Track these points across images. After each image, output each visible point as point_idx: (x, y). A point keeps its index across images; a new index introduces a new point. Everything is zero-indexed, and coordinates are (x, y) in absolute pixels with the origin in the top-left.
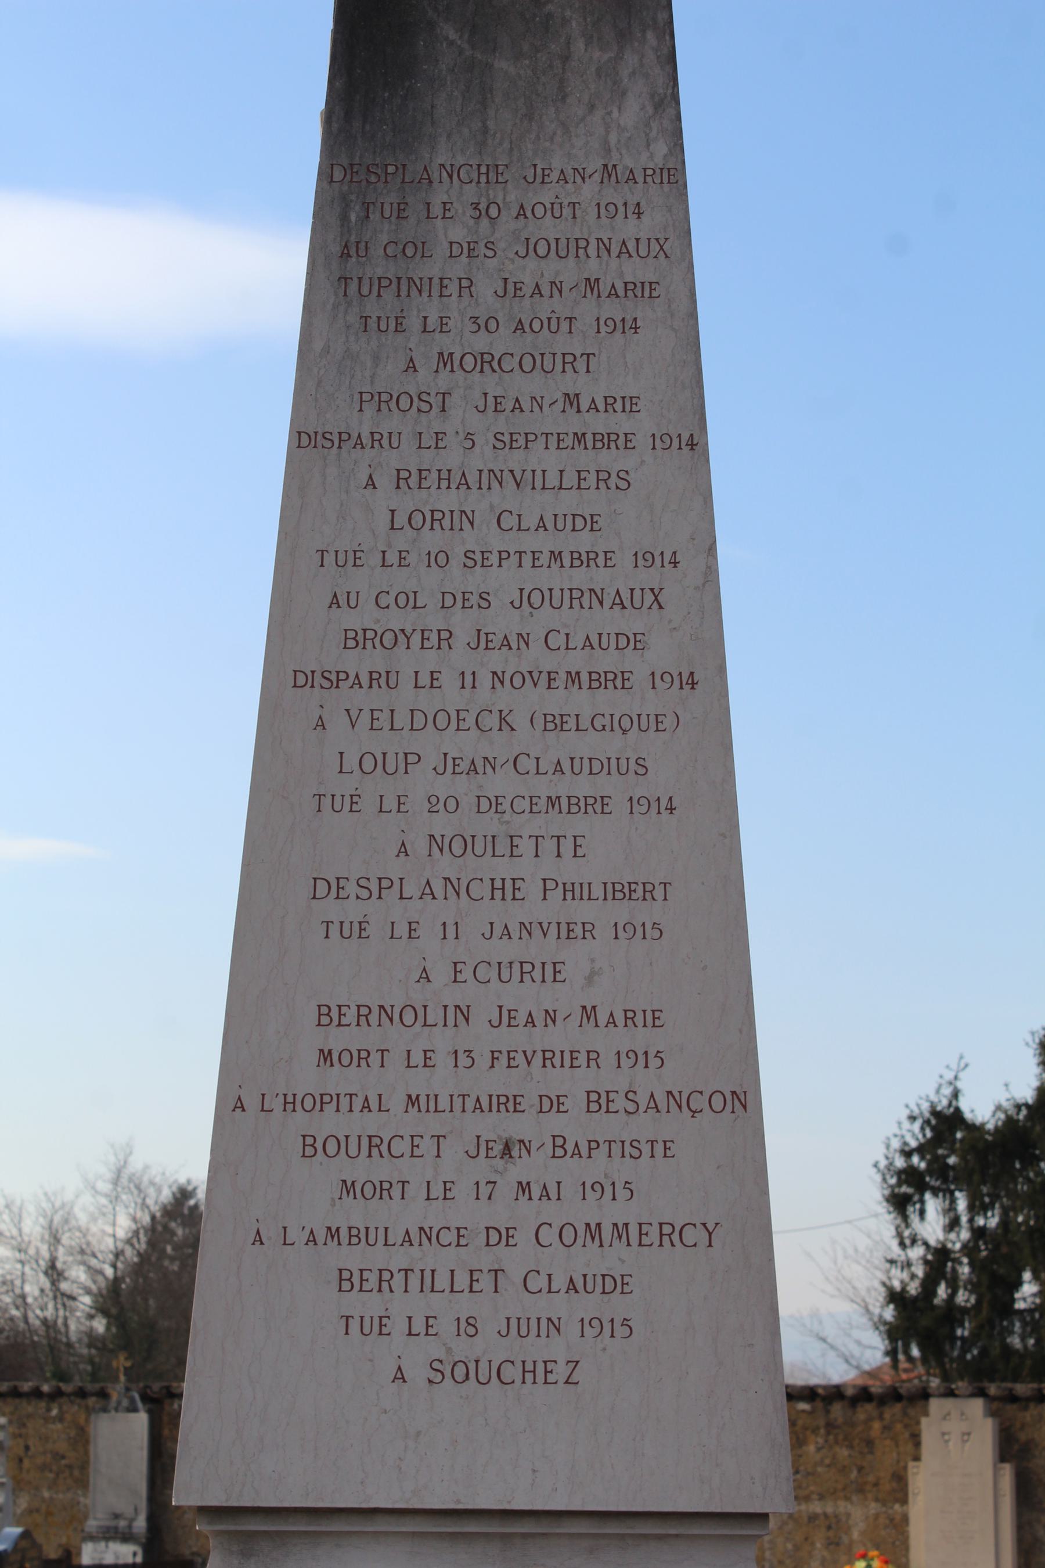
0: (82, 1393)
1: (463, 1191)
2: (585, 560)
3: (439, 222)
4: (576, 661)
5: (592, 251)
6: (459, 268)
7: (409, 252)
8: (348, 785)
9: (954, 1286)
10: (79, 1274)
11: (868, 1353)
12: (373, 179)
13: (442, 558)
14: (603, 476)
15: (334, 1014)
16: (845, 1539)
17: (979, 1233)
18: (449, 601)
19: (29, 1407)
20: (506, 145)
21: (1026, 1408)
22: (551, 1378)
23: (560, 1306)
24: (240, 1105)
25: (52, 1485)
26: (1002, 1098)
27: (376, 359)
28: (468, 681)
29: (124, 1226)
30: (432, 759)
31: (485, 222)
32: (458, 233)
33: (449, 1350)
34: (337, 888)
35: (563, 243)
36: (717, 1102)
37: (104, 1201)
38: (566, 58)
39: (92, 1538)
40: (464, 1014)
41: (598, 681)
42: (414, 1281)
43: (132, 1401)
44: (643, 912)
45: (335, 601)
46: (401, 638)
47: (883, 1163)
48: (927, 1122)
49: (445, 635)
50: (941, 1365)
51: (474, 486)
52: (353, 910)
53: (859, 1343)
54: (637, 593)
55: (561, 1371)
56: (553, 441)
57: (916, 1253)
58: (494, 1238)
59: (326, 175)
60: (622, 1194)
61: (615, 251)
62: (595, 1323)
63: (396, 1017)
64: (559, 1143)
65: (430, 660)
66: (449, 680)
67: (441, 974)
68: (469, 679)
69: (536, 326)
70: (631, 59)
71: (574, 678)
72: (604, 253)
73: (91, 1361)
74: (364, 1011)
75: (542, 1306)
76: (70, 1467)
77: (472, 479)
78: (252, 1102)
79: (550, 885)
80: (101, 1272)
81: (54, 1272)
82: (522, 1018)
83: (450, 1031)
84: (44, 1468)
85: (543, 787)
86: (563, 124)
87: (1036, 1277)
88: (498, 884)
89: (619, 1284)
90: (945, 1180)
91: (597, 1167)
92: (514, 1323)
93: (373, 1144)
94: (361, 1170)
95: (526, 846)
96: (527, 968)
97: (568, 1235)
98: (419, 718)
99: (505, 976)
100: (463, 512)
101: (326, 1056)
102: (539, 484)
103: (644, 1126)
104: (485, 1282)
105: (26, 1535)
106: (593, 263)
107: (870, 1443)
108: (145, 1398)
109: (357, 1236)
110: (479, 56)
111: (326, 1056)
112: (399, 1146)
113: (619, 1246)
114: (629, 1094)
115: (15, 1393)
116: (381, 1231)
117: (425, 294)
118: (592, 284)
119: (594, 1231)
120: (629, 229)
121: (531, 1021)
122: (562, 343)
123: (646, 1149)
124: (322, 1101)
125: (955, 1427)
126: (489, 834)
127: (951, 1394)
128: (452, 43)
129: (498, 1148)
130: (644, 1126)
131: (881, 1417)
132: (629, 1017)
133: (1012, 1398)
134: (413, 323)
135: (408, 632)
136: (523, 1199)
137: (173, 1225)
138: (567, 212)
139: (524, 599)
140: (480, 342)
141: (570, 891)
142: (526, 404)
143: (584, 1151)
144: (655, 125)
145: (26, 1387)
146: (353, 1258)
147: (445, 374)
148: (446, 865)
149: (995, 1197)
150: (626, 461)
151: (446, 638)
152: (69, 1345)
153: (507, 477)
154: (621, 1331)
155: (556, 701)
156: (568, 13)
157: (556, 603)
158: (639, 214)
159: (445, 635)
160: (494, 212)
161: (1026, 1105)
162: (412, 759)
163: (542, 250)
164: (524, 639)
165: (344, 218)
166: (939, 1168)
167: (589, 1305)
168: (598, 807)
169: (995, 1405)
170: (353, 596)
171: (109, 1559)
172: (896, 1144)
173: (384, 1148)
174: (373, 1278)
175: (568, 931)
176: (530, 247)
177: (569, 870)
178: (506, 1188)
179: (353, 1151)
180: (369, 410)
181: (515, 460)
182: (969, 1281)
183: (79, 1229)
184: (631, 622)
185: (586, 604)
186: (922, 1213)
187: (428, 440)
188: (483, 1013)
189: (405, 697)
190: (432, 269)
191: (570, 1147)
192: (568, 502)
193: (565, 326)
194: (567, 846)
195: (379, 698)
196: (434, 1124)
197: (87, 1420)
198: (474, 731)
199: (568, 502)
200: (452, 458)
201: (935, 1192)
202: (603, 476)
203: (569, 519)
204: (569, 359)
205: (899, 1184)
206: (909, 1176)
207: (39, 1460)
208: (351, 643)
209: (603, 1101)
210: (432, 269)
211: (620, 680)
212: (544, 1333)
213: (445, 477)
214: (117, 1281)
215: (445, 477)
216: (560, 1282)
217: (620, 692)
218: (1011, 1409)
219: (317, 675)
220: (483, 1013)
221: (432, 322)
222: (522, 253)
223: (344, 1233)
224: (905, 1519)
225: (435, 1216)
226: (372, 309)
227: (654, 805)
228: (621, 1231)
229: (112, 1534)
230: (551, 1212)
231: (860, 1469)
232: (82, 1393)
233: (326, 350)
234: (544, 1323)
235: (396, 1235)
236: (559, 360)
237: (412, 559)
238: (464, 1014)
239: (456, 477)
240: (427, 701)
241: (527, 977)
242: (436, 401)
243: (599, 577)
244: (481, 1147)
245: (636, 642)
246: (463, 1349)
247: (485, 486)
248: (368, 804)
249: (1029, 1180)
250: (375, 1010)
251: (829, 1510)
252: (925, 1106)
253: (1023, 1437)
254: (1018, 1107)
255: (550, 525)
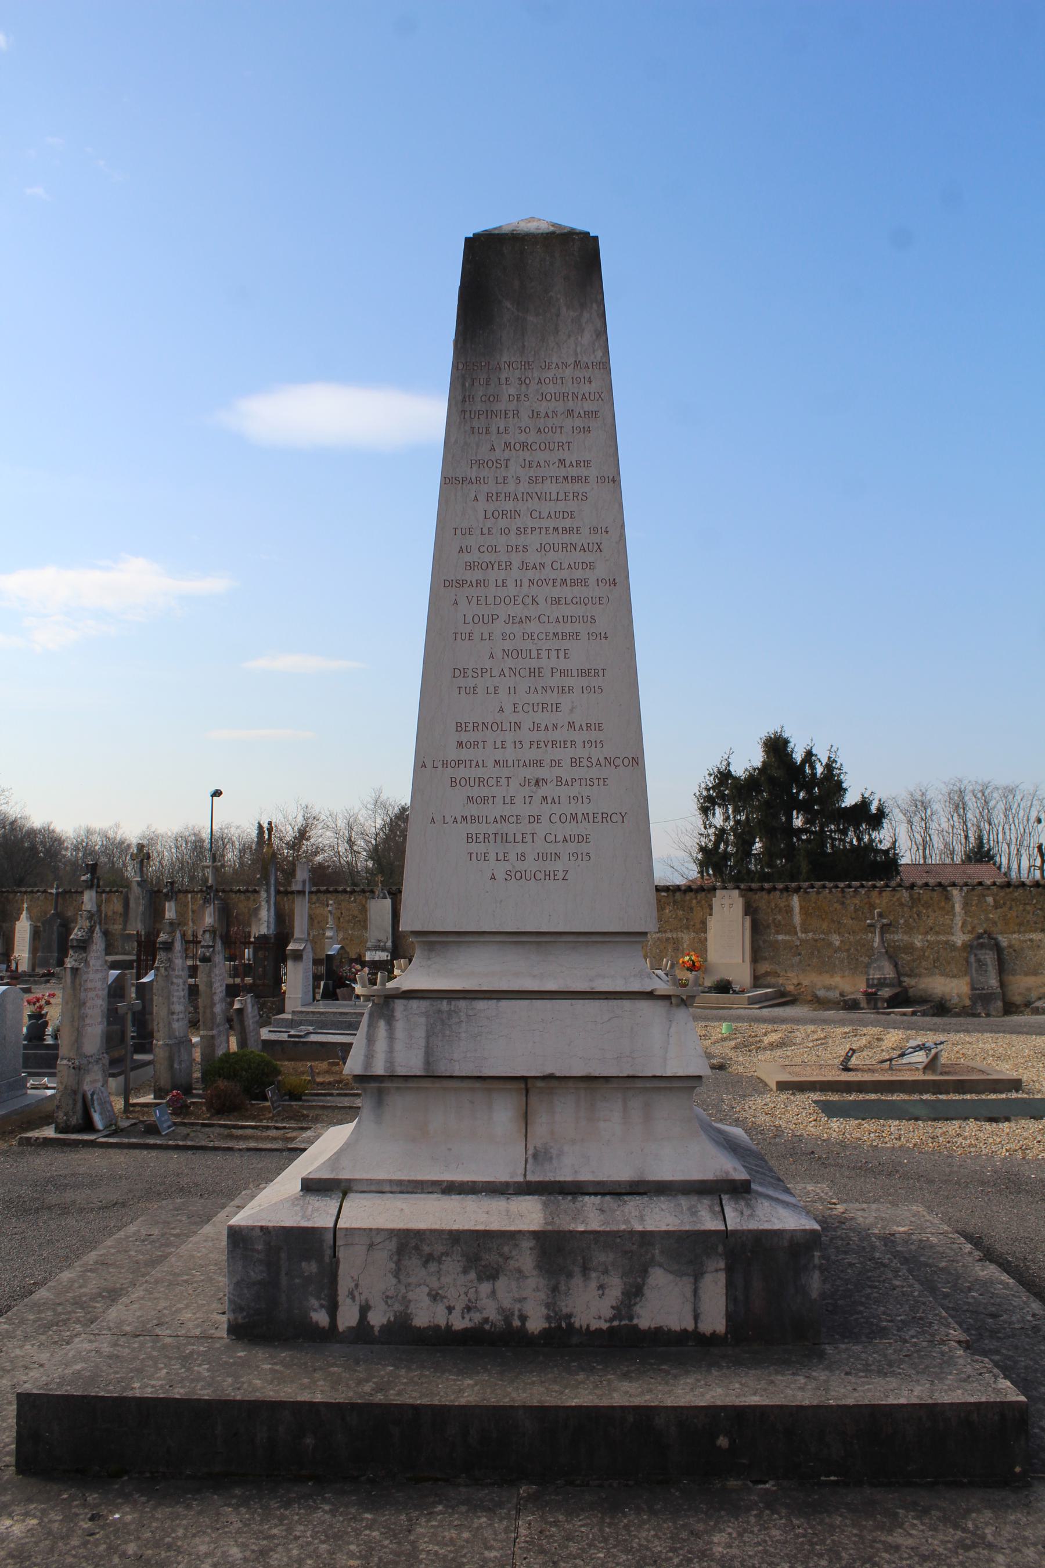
0: (363, 891)
1: (519, 800)
2: (569, 531)
3: (504, 386)
4: (565, 574)
5: (570, 398)
6: (512, 406)
7: (492, 399)
8: (468, 628)
9: (727, 844)
10: (361, 843)
11: (691, 872)
12: (476, 368)
13: (507, 531)
14: (576, 494)
15: (463, 726)
16: (681, 948)
17: (737, 822)
18: (510, 549)
19: (342, 897)
20: (533, 353)
21: (756, 894)
22: (556, 878)
23: (559, 848)
24: (424, 765)
25: (353, 929)
26: (748, 766)
27: (478, 446)
28: (518, 583)
29: (379, 823)
30: (503, 617)
31: (524, 386)
32: (512, 391)
33: (514, 867)
34: (464, 672)
35: (557, 395)
36: (626, 762)
37: (371, 812)
38: (558, 315)
39: (369, 950)
40: (518, 725)
41: (574, 583)
42: (499, 838)
43: (384, 894)
44: (595, 682)
45: (461, 550)
46: (490, 565)
47: (698, 794)
48: (717, 776)
49: (508, 564)
50: (722, 877)
51: (520, 500)
52: (470, 682)
53: (687, 868)
54: (591, 545)
55: (561, 875)
56: (554, 480)
57: (712, 831)
58: (532, 820)
59: (455, 366)
60: (586, 801)
61: (580, 398)
62: (575, 855)
63: (489, 727)
64: (559, 779)
65: (503, 574)
66: (510, 583)
67: (508, 709)
68: (519, 583)
69: (546, 430)
70: (586, 315)
71: (564, 582)
72: (575, 399)
73: (367, 878)
74: (476, 725)
75: (552, 848)
76: (359, 921)
77: (519, 496)
78: (429, 764)
79: (555, 670)
80: (370, 842)
81: (351, 842)
82: (543, 727)
83: (512, 733)
84: (349, 922)
85: (551, 629)
86: (557, 344)
87: (761, 840)
88: (532, 670)
89: (585, 839)
90: (724, 801)
91: (575, 790)
92: (541, 855)
93: (480, 781)
94: (476, 792)
95: (544, 654)
96: (545, 706)
97: (563, 819)
98: (498, 600)
99: (536, 709)
100: (515, 511)
101: (460, 744)
102: (548, 498)
103: (594, 773)
104: (529, 838)
105: (342, 948)
106: (571, 402)
107: (691, 909)
108: (390, 893)
109: (473, 819)
110: (520, 314)
111: (460, 744)
112: (492, 782)
113: (585, 823)
114: (589, 759)
115: (336, 891)
116: (484, 818)
117: (498, 417)
118: (570, 412)
119: (574, 817)
120: (586, 388)
121: (547, 728)
122: (558, 438)
123: (596, 782)
124: (459, 763)
125: (727, 902)
126: (528, 649)
127: (725, 888)
128: (508, 309)
129: (533, 782)
130: (594, 773)
131: (696, 898)
132: (589, 726)
133: (750, 890)
134: (493, 429)
135: (493, 562)
136: (544, 803)
137: (400, 823)
138: (559, 381)
139: (542, 548)
140: (522, 438)
141: (563, 673)
142: (542, 464)
143: (570, 783)
144: (597, 344)
145: (340, 888)
146: (473, 829)
147: (507, 452)
148: (510, 662)
149: (744, 808)
150: (586, 488)
151: (509, 565)
152: (358, 872)
153: (534, 496)
154: (586, 858)
155: (557, 592)
156: (559, 296)
157: (556, 549)
158: (590, 382)
159: (508, 564)
160: (528, 381)
161: (758, 768)
162: (495, 617)
163: (548, 398)
164: (543, 565)
165: (463, 385)
166: (722, 796)
167: (572, 847)
168: (575, 637)
169: (743, 892)
170: (469, 548)
171: (377, 958)
172: (703, 785)
173: (485, 783)
174: (481, 837)
175: (562, 690)
176: (543, 397)
177: (563, 664)
178: (537, 799)
179: (472, 784)
180: (475, 467)
181: (538, 488)
182: (733, 842)
183: (361, 824)
184: (589, 557)
185: (569, 550)
186: (714, 814)
187: (501, 480)
188: (527, 725)
189: (492, 590)
190: (501, 406)
191: (564, 781)
192: (561, 506)
193: (559, 430)
194: (562, 654)
195: (480, 591)
196: (506, 772)
197: (366, 902)
198: (521, 605)
199: (561, 506)
200: (511, 487)
201: (720, 805)
202: (576, 494)
203: (561, 513)
204: (561, 444)
205: (704, 802)
206: (709, 799)
207: (347, 918)
208: (468, 568)
209: (578, 762)
210: (501, 406)
211: (584, 582)
212: (553, 859)
213: (508, 496)
214: (377, 845)
215: (508, 496)
216: (560, 838)
217: (584, 587)
218: (750, 894)
219: (454, 582)
220: (527, 725)
221: (502, 429)
222: (540, 399)
223: (469, 818)
224: (706, 939)
225: (507, 811)
226: (476, 424)
227: (599, 636)
228: (585, 816)
229: (377, 948)
230: (555, 808)
231: (687, 919)
232: (363, 891)
233: (456, 442)
234: (553, 855)
235: (491, 819)
236: (556, 444)
237: (494, 531)
238: (518, 725)
239: (512, 496)
240: (501, 592)
241: (545, 710)
242: (503, 463)
243: (574, 538)
244: (526, 782)
245: (591, 566)
246: (520, 866)
247: (525, 499)
248: (476, 636)
249: (759, 800)
250: (481, 724)
251: (674, 936)
252: (716, 769)
253: (754, 905)
254: (754, 769)
255: (553, 516)
